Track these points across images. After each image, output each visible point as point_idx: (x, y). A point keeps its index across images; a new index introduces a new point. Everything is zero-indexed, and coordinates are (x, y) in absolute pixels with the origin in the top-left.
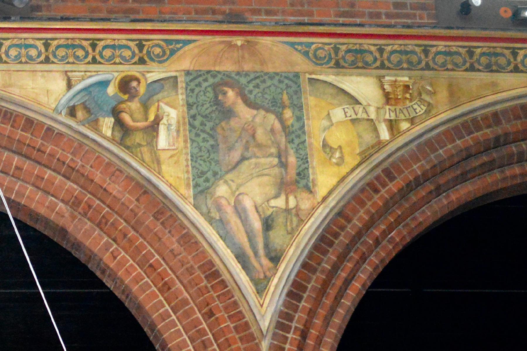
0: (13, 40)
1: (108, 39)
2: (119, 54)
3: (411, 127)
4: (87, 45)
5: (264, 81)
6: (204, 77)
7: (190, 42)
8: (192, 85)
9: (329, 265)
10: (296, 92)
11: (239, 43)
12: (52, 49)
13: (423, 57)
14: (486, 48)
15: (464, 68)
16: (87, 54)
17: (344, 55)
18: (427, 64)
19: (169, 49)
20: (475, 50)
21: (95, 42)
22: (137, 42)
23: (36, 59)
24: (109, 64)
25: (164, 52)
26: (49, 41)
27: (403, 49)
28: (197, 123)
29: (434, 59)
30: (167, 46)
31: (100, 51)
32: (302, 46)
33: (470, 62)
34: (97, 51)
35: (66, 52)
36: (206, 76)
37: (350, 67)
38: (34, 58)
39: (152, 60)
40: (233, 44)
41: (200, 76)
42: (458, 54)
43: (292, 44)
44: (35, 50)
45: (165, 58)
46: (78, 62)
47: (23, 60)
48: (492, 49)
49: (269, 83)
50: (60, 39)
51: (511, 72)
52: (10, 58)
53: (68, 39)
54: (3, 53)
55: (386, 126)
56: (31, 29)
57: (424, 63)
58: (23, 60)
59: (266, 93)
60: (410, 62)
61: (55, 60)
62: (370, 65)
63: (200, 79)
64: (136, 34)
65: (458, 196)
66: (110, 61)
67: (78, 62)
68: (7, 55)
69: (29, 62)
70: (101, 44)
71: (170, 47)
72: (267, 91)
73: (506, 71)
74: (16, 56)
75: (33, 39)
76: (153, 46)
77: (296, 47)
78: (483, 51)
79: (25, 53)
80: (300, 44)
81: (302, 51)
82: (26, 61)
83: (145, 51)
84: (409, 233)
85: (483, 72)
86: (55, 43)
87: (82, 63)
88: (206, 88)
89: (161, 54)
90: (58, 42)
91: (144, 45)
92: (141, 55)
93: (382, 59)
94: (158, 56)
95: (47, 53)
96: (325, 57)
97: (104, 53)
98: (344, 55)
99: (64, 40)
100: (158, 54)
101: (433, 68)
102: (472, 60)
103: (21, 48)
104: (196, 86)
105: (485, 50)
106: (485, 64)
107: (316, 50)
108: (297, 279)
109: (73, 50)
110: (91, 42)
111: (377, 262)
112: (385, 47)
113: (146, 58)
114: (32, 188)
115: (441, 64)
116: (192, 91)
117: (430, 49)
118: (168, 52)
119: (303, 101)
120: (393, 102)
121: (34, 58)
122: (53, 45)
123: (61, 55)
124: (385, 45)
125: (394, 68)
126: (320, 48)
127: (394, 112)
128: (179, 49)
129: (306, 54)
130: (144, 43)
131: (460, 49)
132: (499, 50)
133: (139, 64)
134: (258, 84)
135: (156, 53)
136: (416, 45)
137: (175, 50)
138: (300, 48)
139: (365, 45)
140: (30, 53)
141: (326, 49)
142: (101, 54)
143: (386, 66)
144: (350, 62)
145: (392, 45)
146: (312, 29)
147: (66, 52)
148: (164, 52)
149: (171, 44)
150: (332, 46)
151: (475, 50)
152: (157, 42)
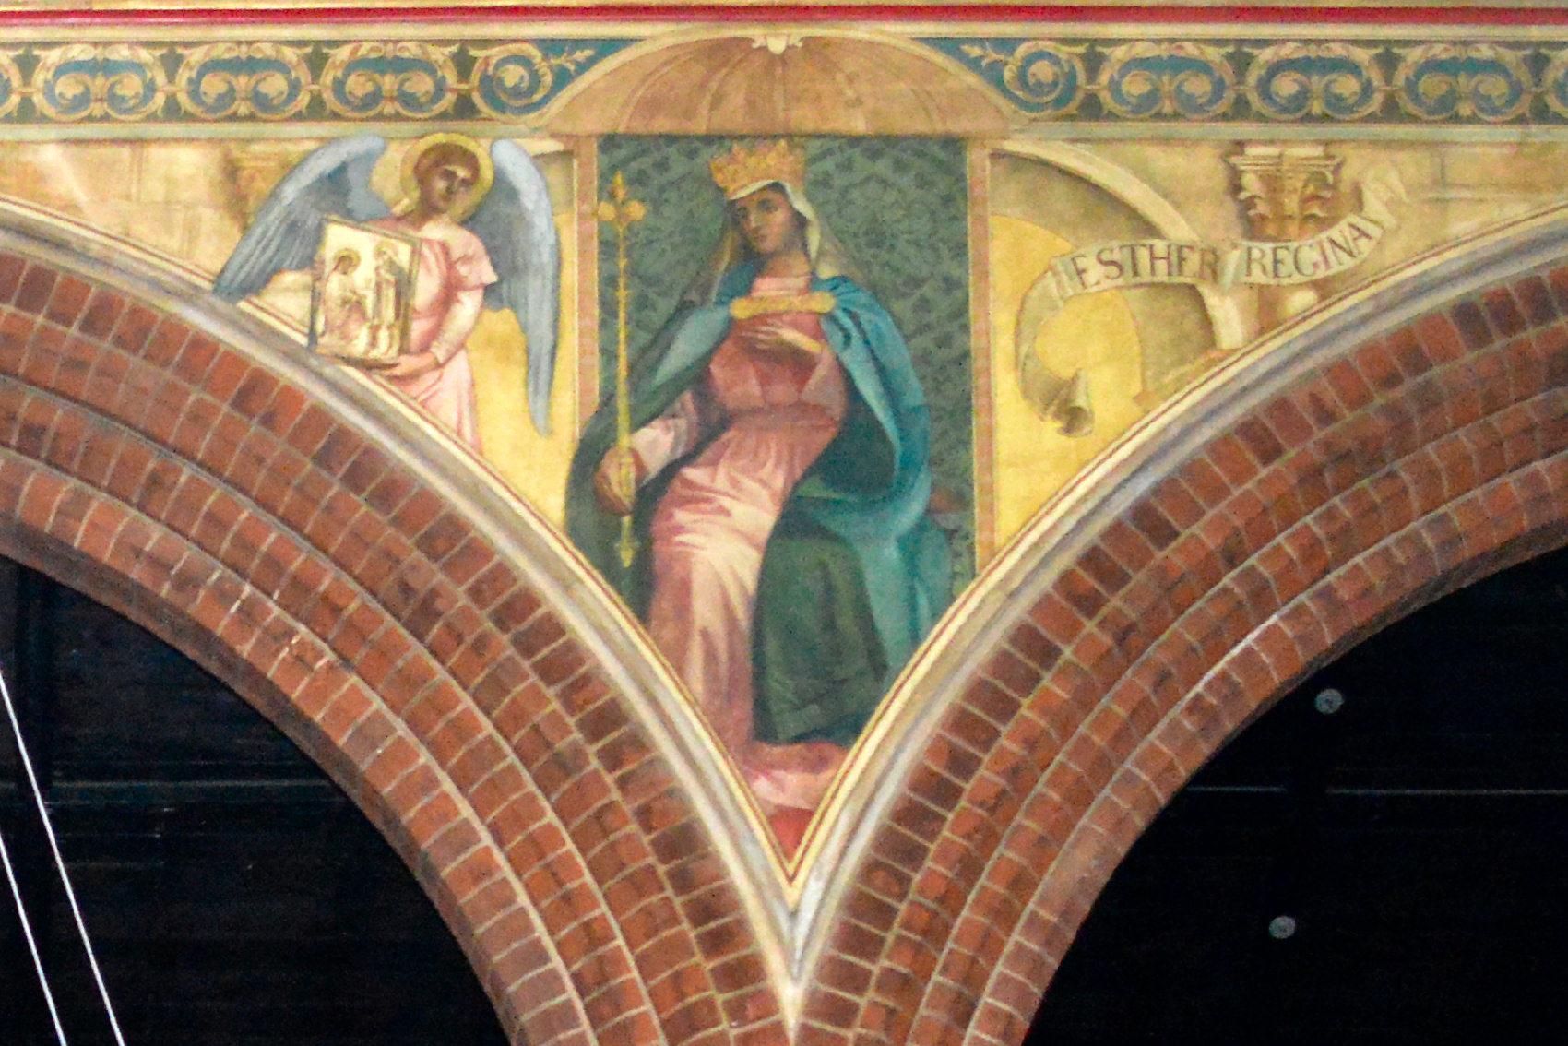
0: (1430, 48)
1: (1289, 40)
2: (1173, 88)
6: (657, 156)
9: (489, 930)
10: (947, 200)
11: (777, 46)
13: (161, 79)
14: (1293, 45)
17: (1116, 77)
18: (26, 102)
20: (1106, 51)
21: (1544, 51)
22: (309, 50)
25: (536, 79)
27: (1313, 56)
30: (546, 58)
32: (983, 47)
33: (21, 93)
36: (849, 152)
37: (64, 118)
38: (275, 102)
39: (501, 107)
40: (755, 46)
41: (644, 152)
42: (277, 65)
43: (948, 45)
45: (537, 97)
46: (349, 114)
47: (1167, 107)
48: (1313, 47)
50: (1283, 41)
54: (1401, 89)
55: (1242, 311)
57: (159, 100)
59: (851, 202)
62: (1351, 109)
65: (148, 584)
70: (196, 56)
71: (554, 61)
72: (672, 195)
74: (220, 97)
75: (1197, 41)
77: (588, 53)
78: (1430, 54)
79: (106, 90)
81: (984, 63)
83: (475, 77)
85: (204, 121)
88: (662, 189)
89: (525, 84)
90: (207, 54)
92: (171, 89)
93: (28, 90)
94: (516, 92)
96: (1055, 84)
98: (1116, 77)
100: (515, 88)
102: (467, 83)
105: (1288, 52)
106: (214, 96)
107: (1030, 60)
109: (107, 79)
110: (163, 51)
111: (1054, 919)
113: (477, 99)
114: (443, 577)
115: (216, 100)
117: (1256, 52)
118: (548, 79)
119: (969, 226)
120: (1271, 230)
121: (275, 102)
124: (187, 45)
125: (203, 116)
126: (1040, 55)
129: (993, 74)
130: (473, 52)
134: (642, 172)
136: (1356, 42)
139: (262, 46)
140: (263, 88)
141: (1063, 56)
142: (1114, 87)
143: (1105, 112)
144: (1432, 102)
145: (209, 43)
149: (558, 55)
150: (1081, 49)
151: (1106, 51)
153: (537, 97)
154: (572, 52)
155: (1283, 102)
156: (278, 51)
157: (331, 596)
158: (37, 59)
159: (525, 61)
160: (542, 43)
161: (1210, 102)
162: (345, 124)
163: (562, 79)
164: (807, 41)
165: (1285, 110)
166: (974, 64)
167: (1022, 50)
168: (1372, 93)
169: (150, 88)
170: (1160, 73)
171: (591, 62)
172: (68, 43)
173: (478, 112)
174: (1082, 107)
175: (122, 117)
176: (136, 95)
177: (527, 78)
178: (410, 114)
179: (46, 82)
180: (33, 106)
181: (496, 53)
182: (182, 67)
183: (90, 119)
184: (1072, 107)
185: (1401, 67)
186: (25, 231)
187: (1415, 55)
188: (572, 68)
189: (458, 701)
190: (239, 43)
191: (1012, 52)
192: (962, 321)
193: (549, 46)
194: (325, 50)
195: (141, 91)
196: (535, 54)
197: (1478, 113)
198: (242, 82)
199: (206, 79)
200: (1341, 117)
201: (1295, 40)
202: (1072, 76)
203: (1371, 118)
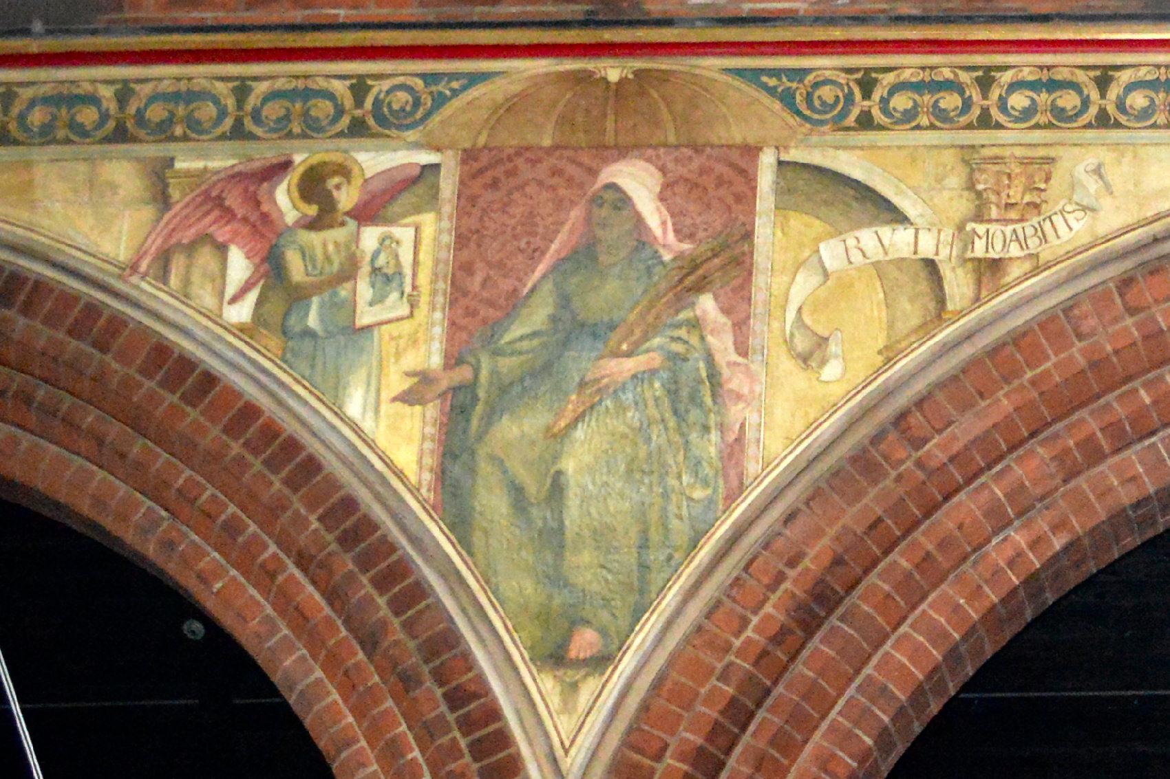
0: (1021, 71)
3: (973, 307)
4: (225, 92)
5: (511, 173)
7: (475, 79)
8: (476, 186)
11: (613, 75)
12: (252, 102)
15: (100, 134)
16: (340, 111)
18: (985, 112)
19: (431, 93)
22: (980, 73)
23: (328, 128)
24: (1145, 128)
26: (249, 83)
28: (475, 283)
29: (884, 101)
31: (138, 110)
32: (780, 79)
34: (876, 96)
35: (915, 101)
41: (500, 161)
44: (94, 109)
46: (1010, 125)
47: (178, 131)
49: (526, 172)
50: (160, 79)
51: (223, 137)
52: (892, 116)
53: (1158, 66)
56: (751, 45)
57: (976, 112)
58: (297, 129)
60: (74, 126)
61: (258, 131)
63: (499, 172)
64: (721, 54)
66: (909, 121)
67: (194, 135)
68: (885, 111)
69: (938, 124)
73: (956, 125)
74: (279, 120)
76: (388, 93)
77: (765, 79)
80: (775, 73)
81: (780, 90)
82: (1050, 121)
84: (1034, 544)
86: (890, 78)
87: (1075, 125)
91: (371, 87)
92: (358, 113)
93: (986, 102)
95: (986, 102)
97: (1128, 102)
99: (1032, 68)
101: (997, 122)
103: (293, 102)
104: (486, 186)
108: (470, 675)
110: (236, 83)
112: (137, 87)
113: (371, 122)
116: (473, 200)
122: (885, 83)
123: (274, 118)
124: (21, 84)
126: (826, 82)
127: (984, 239)
128: (455, 93)
129: (787, 99)
131: (1079, 72)
132: (1062, 75)
133: (1098, 128)
135: (396, 107)
137: (445, 96)
138: (772, 82)
139: (318, 79)
142: (1003, 105)
146: (820, 34)
147: (915, 101)
148: (417, 103)
150: (859, 75)
152: (401, 79)
153: (419, 115)
154: (449, 82)
155: (1017, 114)
156: (1072, 74)
157: (916, 561)
158: (876, 80)
159: (409, 89)
160: (423, 76)
161: (96, 129)
162: (938, 132)
163: (440, 101)
164: (638, 73)
165: (1017, 120)
166: (771, 91)
167: (810, 78)
168: (135, 116)
169: (1086, 103)
170: (1039, 92)
171: (464, 88)
172: (900, 68)
173: (368, 128)
174: (858, 120)
175: (1063, 125)
176: (1075, 107)
177: (410, 99)
178: (1059, 124)
179: (1118, 97)
180: (990, 116)
181: (386, 85)
182: (995, 85)
183: (1037, 126)
184: (851, 120)
185: (17, 102)
186: (15, 248)
187: (262, 88)
188: (448, 93)
189: (328, 693)
190: (297, 77)
191: (801, 81)
192: (745, 293)
193: (426, 77)
194: (874, 75)
195: (960, 106)
196: (419, 83)
197: (188, 132)
198: (1043, 98)
199: (270, 104)
200: (201, 137)
201: (170, 78)
202: (851, 93)
203: (969, 127)
